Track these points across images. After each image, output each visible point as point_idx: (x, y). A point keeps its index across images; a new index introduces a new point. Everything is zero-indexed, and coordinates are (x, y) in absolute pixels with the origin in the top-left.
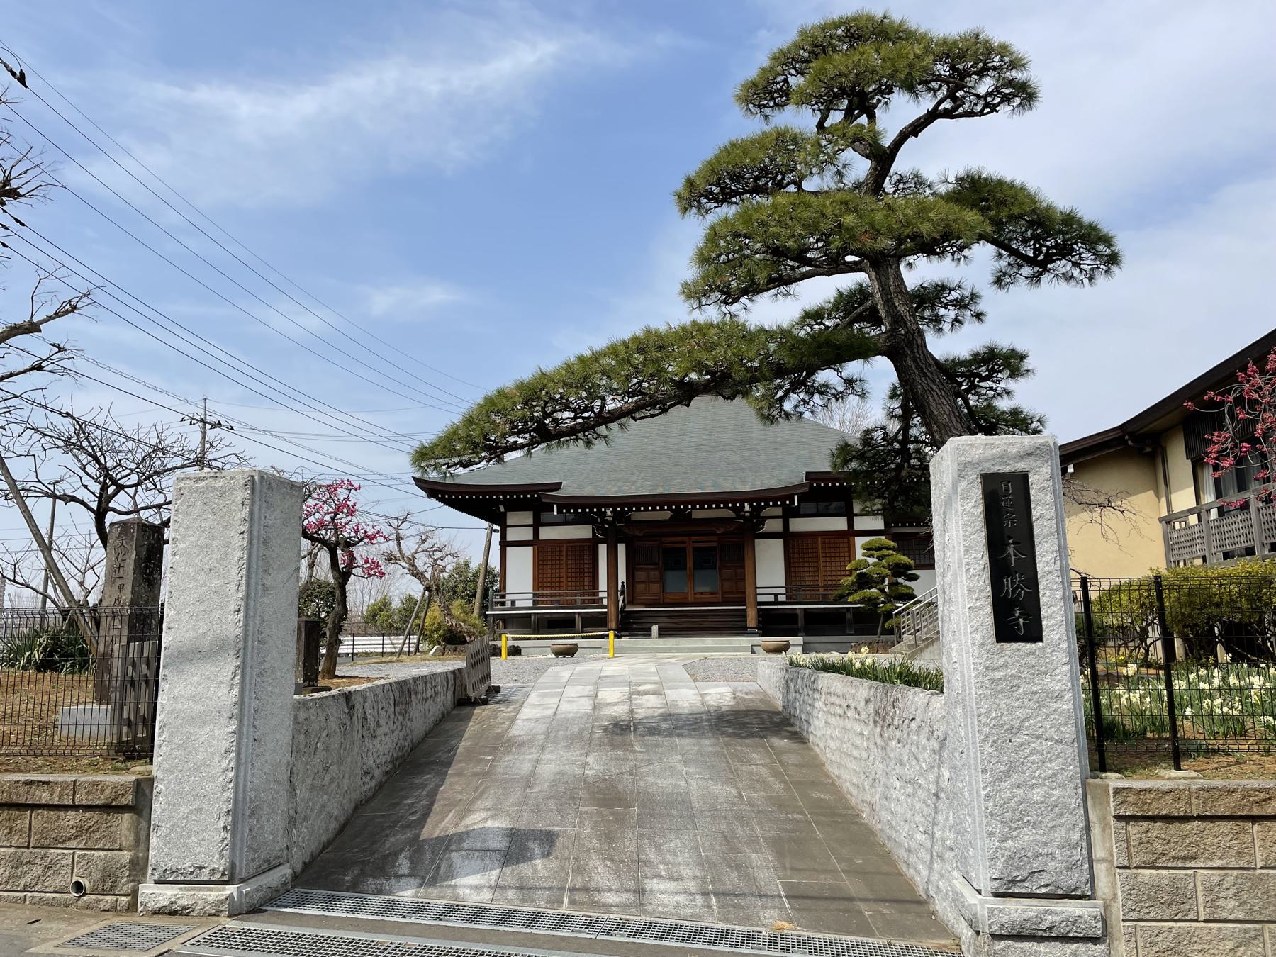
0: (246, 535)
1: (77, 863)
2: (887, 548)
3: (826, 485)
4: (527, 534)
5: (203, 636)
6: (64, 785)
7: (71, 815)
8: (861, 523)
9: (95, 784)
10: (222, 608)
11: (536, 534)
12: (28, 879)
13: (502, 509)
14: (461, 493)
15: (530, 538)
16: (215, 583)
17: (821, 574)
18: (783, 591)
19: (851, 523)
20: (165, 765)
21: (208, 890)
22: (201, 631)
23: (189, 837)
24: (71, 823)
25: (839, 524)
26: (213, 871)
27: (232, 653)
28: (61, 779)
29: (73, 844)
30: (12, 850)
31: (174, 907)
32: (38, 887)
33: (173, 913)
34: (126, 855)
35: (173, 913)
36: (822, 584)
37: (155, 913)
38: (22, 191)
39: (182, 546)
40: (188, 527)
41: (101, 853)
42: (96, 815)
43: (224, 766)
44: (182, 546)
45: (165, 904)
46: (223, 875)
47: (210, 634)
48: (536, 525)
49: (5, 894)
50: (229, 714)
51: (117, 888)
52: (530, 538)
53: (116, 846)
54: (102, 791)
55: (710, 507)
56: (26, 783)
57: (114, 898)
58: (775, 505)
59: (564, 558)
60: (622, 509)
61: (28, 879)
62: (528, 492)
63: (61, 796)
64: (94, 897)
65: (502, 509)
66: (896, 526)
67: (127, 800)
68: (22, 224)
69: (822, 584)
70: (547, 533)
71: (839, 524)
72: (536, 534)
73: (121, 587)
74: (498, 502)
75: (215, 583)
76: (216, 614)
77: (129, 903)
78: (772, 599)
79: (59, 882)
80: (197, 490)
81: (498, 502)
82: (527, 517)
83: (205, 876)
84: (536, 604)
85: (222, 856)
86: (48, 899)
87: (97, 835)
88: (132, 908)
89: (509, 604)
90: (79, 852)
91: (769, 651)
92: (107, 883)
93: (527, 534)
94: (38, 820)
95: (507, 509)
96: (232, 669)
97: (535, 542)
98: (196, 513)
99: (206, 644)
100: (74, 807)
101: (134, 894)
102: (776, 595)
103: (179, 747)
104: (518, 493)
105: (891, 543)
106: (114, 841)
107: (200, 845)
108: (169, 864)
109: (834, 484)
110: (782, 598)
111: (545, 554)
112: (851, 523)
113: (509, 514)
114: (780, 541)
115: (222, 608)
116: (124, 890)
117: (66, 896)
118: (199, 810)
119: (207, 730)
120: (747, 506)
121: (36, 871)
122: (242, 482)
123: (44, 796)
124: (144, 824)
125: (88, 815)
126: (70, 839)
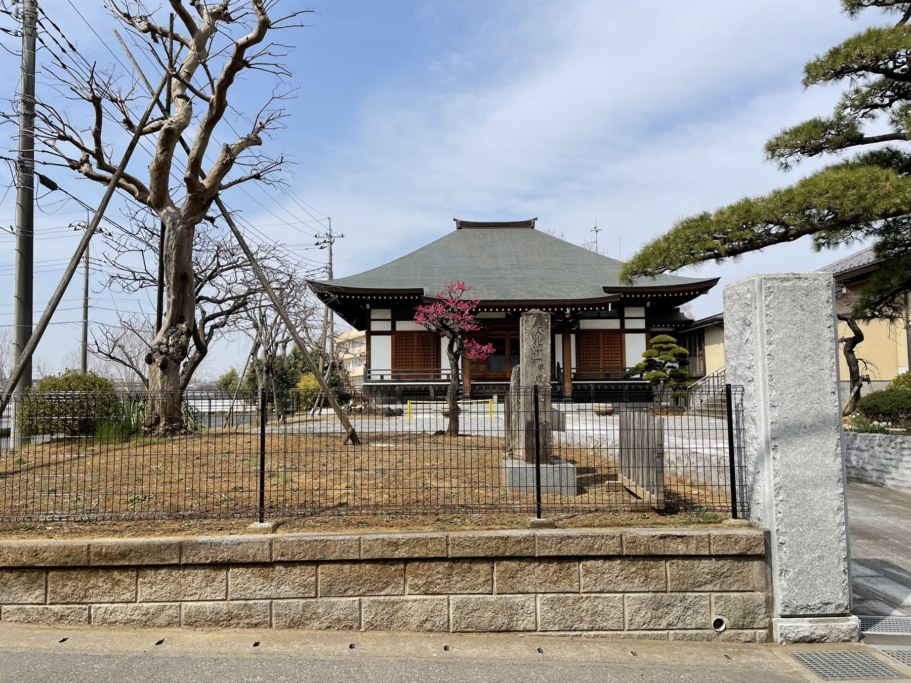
0: (832, 329)
1: (711, 606)
2: (672, 343)
3: (404, 298)
4: (387, 326)
5: (806, 413)
6: (700, 539)
7: (706, 563)
8: (629, 324)
9: (728, 537)
10: (820, 390)
11: (394, 326)
12: (670, 618)
13: (368, 306)
14: (353, 294)
15: (389, 329)
16: (811, 369)
17: (602, 359)
18: (390, 372)
19: (622, 324)
20: (786, 520)
21: (834, 621)
22: (803, 409)
23: (815, 579)
24: (706, 570)
25: (614, 324)
26: (839, 606)
27: (834, 428)
28: (696, 533)
29: (709, 587)
30: (650, 595)
31: (814, 636)
32: (680, 625)
33: (812, 641)
34: (760, 596)
35: (812, 641)
36: (601, 366)
37: (795, 642)
38: (233, 16)
39: (777, 336)
40: (781, 321)
41: (736, 594)
42: (728, 563)
43: (838, 521)
44: (777, 336)
45: (806, 634)
46: (846, 608)
47: (812, 412)
48: (393, 322)
49: (649, 632)
50: (837, 479)
51: (752, 622)
52: (389, 329)
53: (749, 589)
54: (736, 543)
55: (494, 311)
56: (663, 537)
57: (753, 631)
58: (500, 311)
59: (415, 344)
60: (518, 310)
61: (670, 618)
62: (396, 295)
63: (697, 548)
64: (734, 631)
65: (368, 306)
66: (656, 326)
67: (760, 550)
68: (74, 49)
69: (601, 366)
70: (402, 326)
71: (614, 324)
72: (394, 326)
73: (541, 367)
74: (365, 302)
75: (811, 369)
76: (816, 395)
77: (767, 634)
78: (379, 378)
79: (700, 620)
80: (785, 289)
81: (365, 302)
82: (387, 314)
83: (830, 610)
84: (395, 378)
85: (844, 594)
86: (691, 635)
87: (731, 580)
88: (769, 638)
89: (444, 377)
90: (714, 595)
91: (600, 413)
92: (745, 622)
93: (387, 326)
94: (668, 569)
95: (371, 307)
96: (835, 441)
97: (393, 332)
98: (786, 308)
99: (809, 420)
100: (709, 557)
101: (770, 627)
102: (448, 375)
103: (797, 505)
104: (404, 295)
105: (674, 340)
106: (748, 584)
107: (826, 586)
108: (801, 602)
109: (630, 296)
110: (389, 378)
111: (400, 341)
112: (622, 324)
113: (372, 311)
114: (644, 335)
115: (820, 390)
116: (762, 624)
117: (708, 632)
118: (821, 558)
119: (820, 491)
120: (568, 311)
121: (676, 611)
122: (825, 284)
123: (681, 549)
124: (769, 569)
125: (720, 563)
126: (705, 583)
